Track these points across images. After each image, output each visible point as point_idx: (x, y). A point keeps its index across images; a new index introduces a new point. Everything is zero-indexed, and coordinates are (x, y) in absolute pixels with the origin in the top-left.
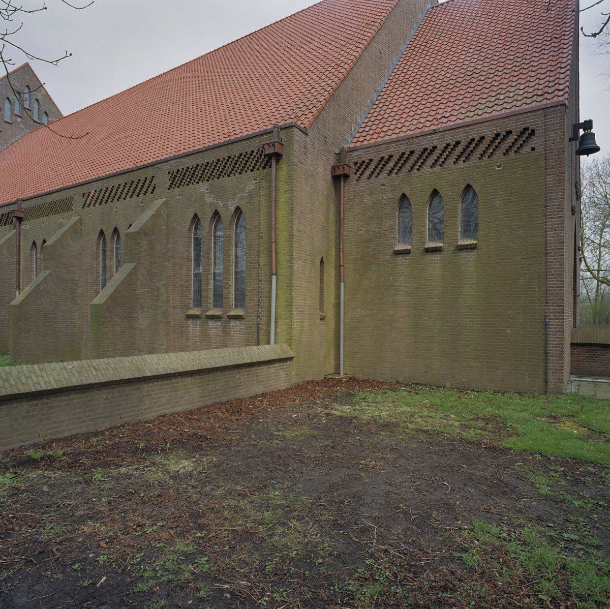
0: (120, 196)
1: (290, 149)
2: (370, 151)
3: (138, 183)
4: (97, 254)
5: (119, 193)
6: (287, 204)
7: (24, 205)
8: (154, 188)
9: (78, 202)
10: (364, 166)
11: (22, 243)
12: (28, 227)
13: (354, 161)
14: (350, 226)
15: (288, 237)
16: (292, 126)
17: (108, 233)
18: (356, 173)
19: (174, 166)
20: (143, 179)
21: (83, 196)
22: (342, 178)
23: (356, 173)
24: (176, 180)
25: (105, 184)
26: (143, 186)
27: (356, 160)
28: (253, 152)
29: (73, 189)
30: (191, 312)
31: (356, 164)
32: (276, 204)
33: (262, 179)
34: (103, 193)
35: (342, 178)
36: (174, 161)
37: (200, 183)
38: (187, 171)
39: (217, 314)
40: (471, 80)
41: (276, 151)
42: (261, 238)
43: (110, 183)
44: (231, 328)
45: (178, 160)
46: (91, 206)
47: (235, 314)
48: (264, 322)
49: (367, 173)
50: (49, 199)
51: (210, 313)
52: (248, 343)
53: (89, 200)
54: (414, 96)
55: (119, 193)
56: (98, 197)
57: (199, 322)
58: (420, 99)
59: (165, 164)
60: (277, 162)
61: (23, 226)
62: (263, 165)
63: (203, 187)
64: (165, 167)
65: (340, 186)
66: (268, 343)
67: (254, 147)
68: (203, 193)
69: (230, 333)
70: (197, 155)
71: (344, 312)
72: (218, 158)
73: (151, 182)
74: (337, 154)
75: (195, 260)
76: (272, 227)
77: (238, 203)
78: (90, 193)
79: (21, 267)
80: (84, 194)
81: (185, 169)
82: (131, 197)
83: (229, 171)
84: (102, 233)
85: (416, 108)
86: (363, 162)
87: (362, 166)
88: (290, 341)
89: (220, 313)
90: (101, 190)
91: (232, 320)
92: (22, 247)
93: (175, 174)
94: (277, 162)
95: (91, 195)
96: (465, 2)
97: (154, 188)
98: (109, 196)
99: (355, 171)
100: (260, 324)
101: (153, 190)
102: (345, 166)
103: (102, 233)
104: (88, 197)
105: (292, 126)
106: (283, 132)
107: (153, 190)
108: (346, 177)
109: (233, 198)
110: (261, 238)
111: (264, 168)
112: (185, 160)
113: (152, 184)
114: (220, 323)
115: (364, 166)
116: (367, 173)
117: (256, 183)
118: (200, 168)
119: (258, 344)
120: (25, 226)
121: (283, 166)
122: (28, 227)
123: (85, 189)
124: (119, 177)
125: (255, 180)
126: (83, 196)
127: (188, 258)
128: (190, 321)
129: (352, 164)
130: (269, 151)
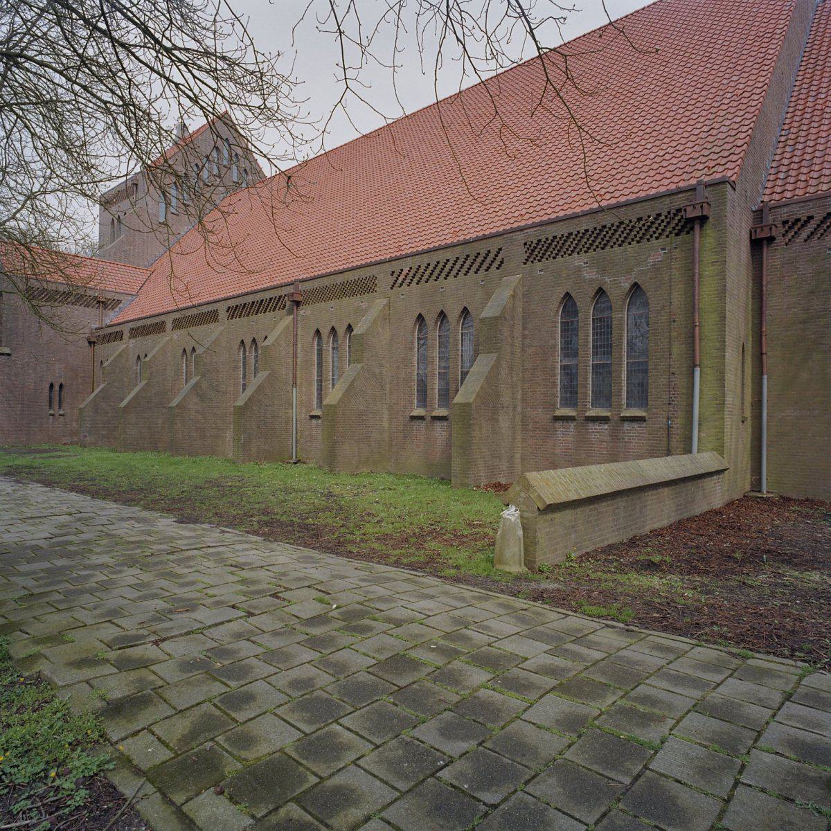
0: (449, 273)
1: (721, 210)
2: (809, 205)
3: (477, 257)
4: (412, 343)
5: (447, 270)
6: (717, 278)
7: (302, 287)
8: (502, 262)
9: (384, 281)
10: (799, 225)
11: (299, 332)
12: (309, 312)
13: (783, 219)
14: (776, 302)
15: (718, 319)
16: (724, 182)
17: (430, 319)
18: (784, 235)
19: (533, 236)
20: (483, 253)
21: (392, 275)
22: (765, 242)
23: (784, 235)
24: (536, 253)
25: (425, 259)
26: (483, 261)
27: (785, 219)
28: (659, 215)
29: (377, 266)
30: (559, 413)
31: (785, 223)
32: (699, 278)
33: (675, 248)
34: (422, 270)
35: (765, 242)
36: (531, 230)
37: (575, 255)
38: (552, 241)
39: (570, 414)
40: (750, 104)
41: (705, 213)
42: (674, 321)
43: (442, 256)
44: (624, 433)
45: (540, 228)
46: (404, 286)
47: (632, 415)
48: (678, 425)
49: (804, 234)
50: (339, 279)
51: (591, 413)
52: (652, 453)
53: (401, 279)
54: (682, 125)
55: (447, 270)
56: (415, 275)
57: (572, 425)
58: (675, 128)
59: (518, 233)
60: (701, 226)
61: (302, 312)
62: (676, 231)
63: (578, 260)
64: (520, 237)
65: (762, 252)
66: (688, 450)
67: (662, 209)
68: (579, 269)
69: (623, 439)
70: (571, 221)
71: (700, 405)
72: (604, 224)
73: (496, 256)
74: (753, 212)
75: (561, 348)
76: (691, 307)
77: (635, 278)
78: (402, 270)
79: (298, 360)
80: (393, 272)
81: (550, 238)
82: (476, 273)
83: (620, 239)
84: (420, 318)
85: (640, 138)
86: (798, 220)
87: (794, 225)
88: (720, 450)
89: (574, 414)
90: (420, 266)
91: (627, 423)
92: (299, 337)
93: (534, 245)
94: (701, 226)
95: (404, 273)
96: (780, 3)
97: (502, 262)
98: (431, 274)
99: (783, 231)
100: (673, 427)
101: (500, 265)
102: (773, 227)
103: (420, 318)
104: (399, 276)
105: (724, 182)
106: (708, 189)
107: (500, 265)
108: (771, 240)
109: (627, 272)
110: (674, 321)
111: (677, 235)
112: (549, 228)
113: (499, 259)
114: (606, 426)
115: (799, 225)
116: (804, 234)
117: (665, 253)
118: (574, 236)
119: (669, 453)
120: (304, 311)
121: (709, 229)
122: (309, 312)
123: (396, 266)
124: (448, 250)
125: (662, 249)
126: (392, 275)
127: (554, 346)
128: (558, 424)
129: (780, 225)
130: (691, 213)
